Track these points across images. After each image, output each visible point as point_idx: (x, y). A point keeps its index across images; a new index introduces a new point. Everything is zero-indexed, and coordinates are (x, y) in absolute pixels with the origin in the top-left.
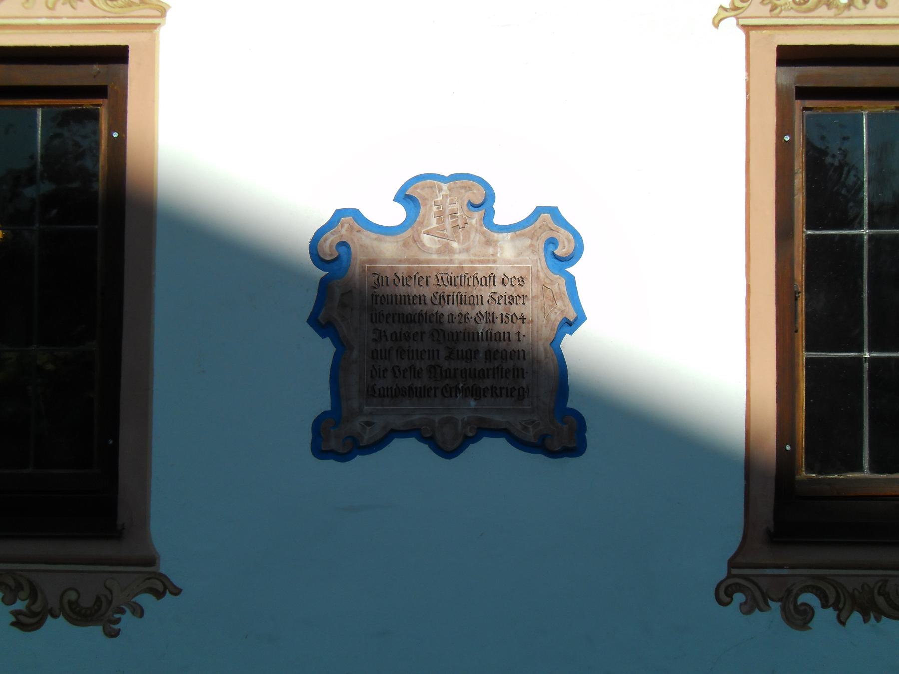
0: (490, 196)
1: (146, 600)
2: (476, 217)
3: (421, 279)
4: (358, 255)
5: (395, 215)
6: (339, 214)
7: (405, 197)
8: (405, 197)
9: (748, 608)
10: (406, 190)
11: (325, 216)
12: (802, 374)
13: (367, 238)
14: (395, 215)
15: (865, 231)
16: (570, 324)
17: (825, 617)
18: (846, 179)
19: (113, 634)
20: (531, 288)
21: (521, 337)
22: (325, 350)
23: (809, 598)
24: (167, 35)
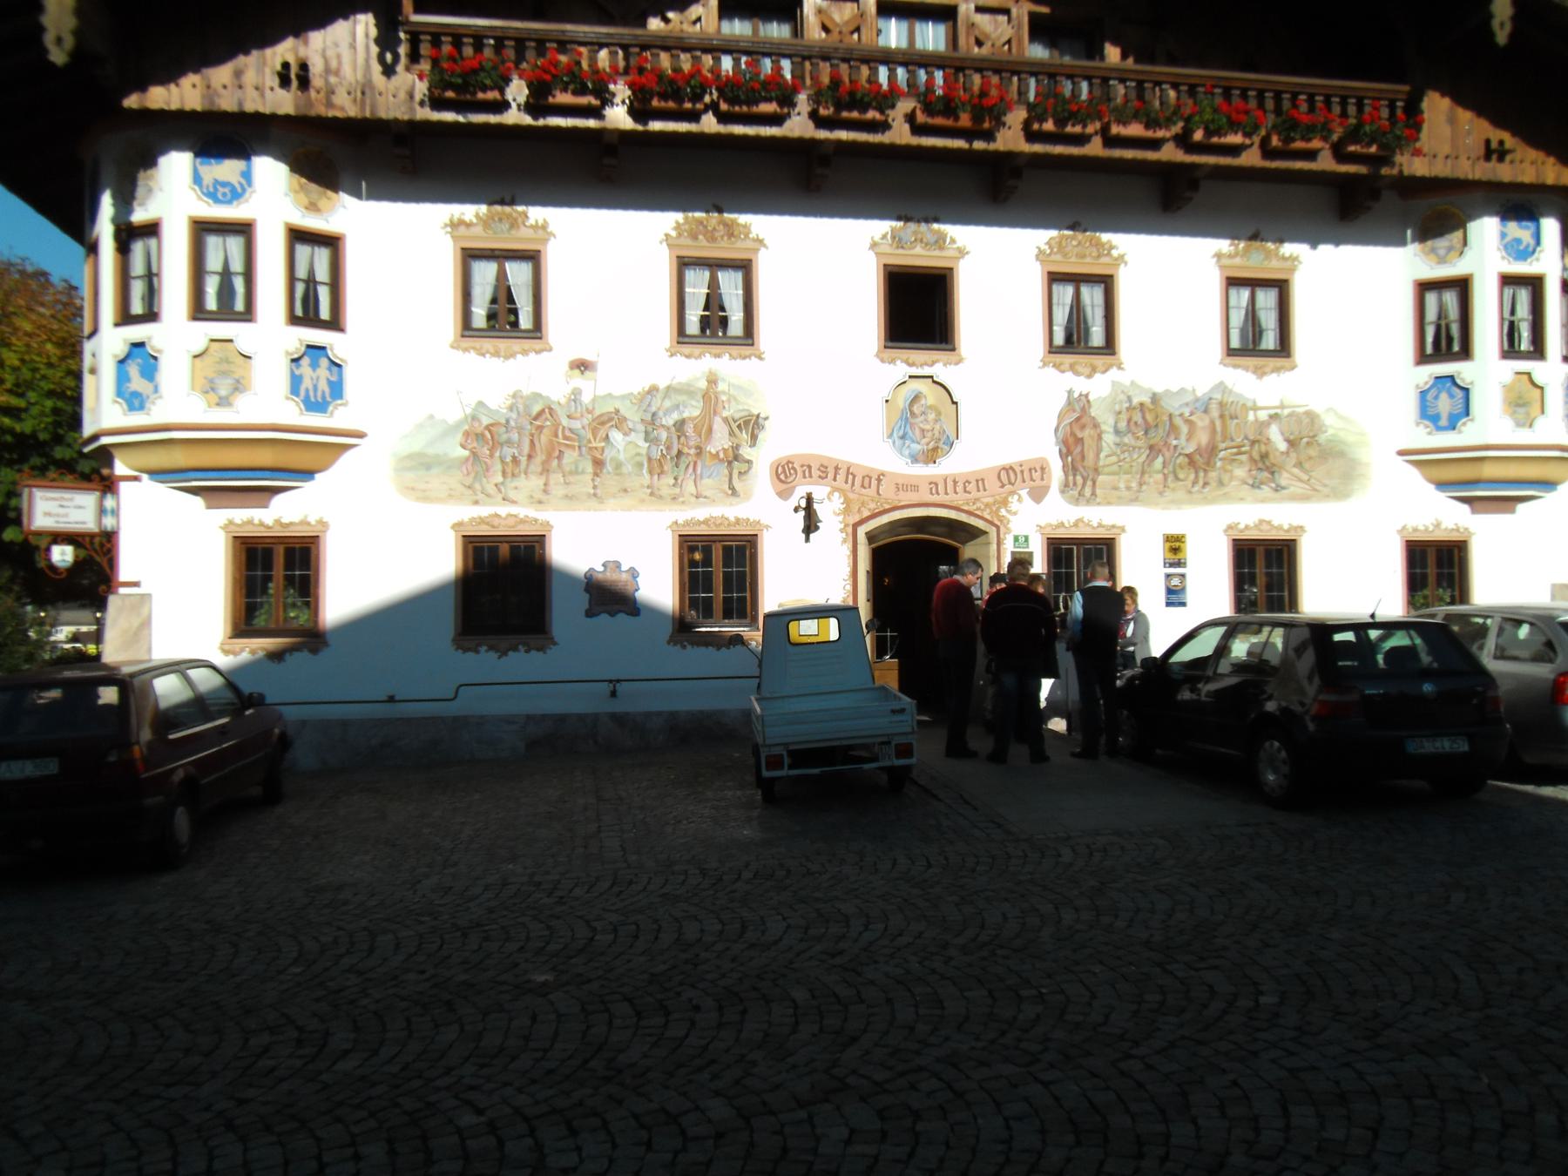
0: (620, 564)
1: (552, 646)
2: (618, 570)
3: (606, 581)
4: (594, 577)
5: (601, 569)
6: (590, 569)
7: (603, 565)
8: (603, 565)
9: (675, 645)
10: (1134, 623)
11: (587, 569)
12: (687, 602)
13: (596, 574)
14: (601, 569)
15: (259, 573)
16: (637, 590)
17: (689, 647)
18: (1520, 346)
19: (545, 653)
20: (629, 583)
21: (760, 420)
22: (588, 595)
23: (686, 643)
24: (553, 532)
